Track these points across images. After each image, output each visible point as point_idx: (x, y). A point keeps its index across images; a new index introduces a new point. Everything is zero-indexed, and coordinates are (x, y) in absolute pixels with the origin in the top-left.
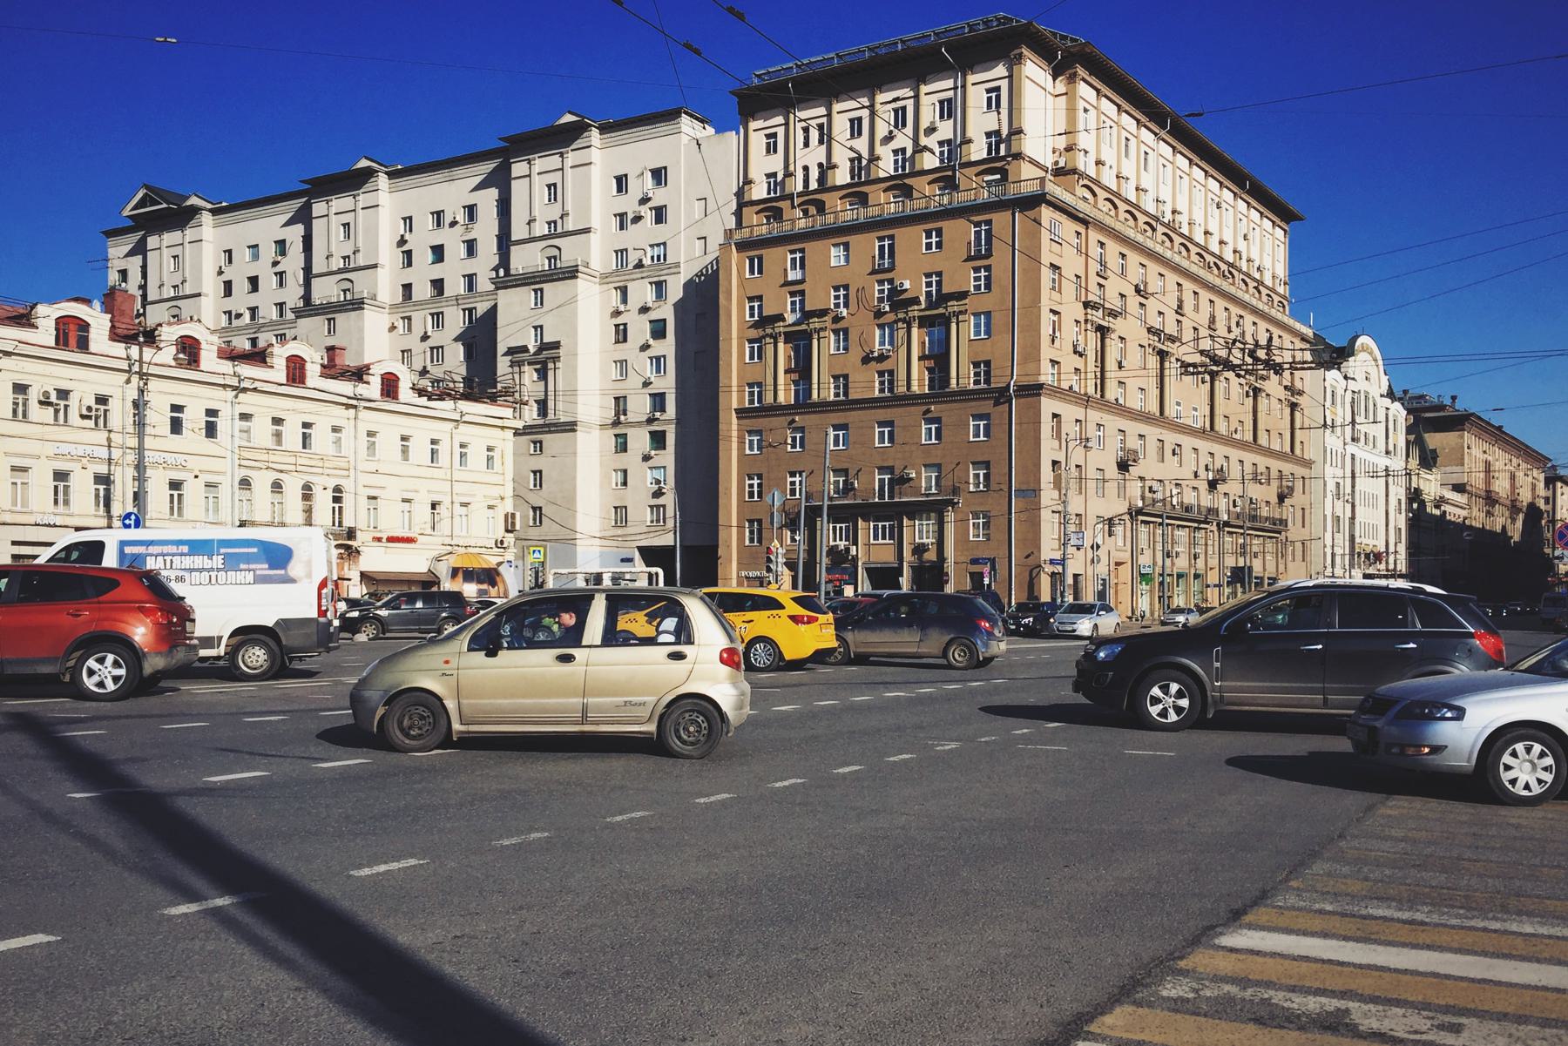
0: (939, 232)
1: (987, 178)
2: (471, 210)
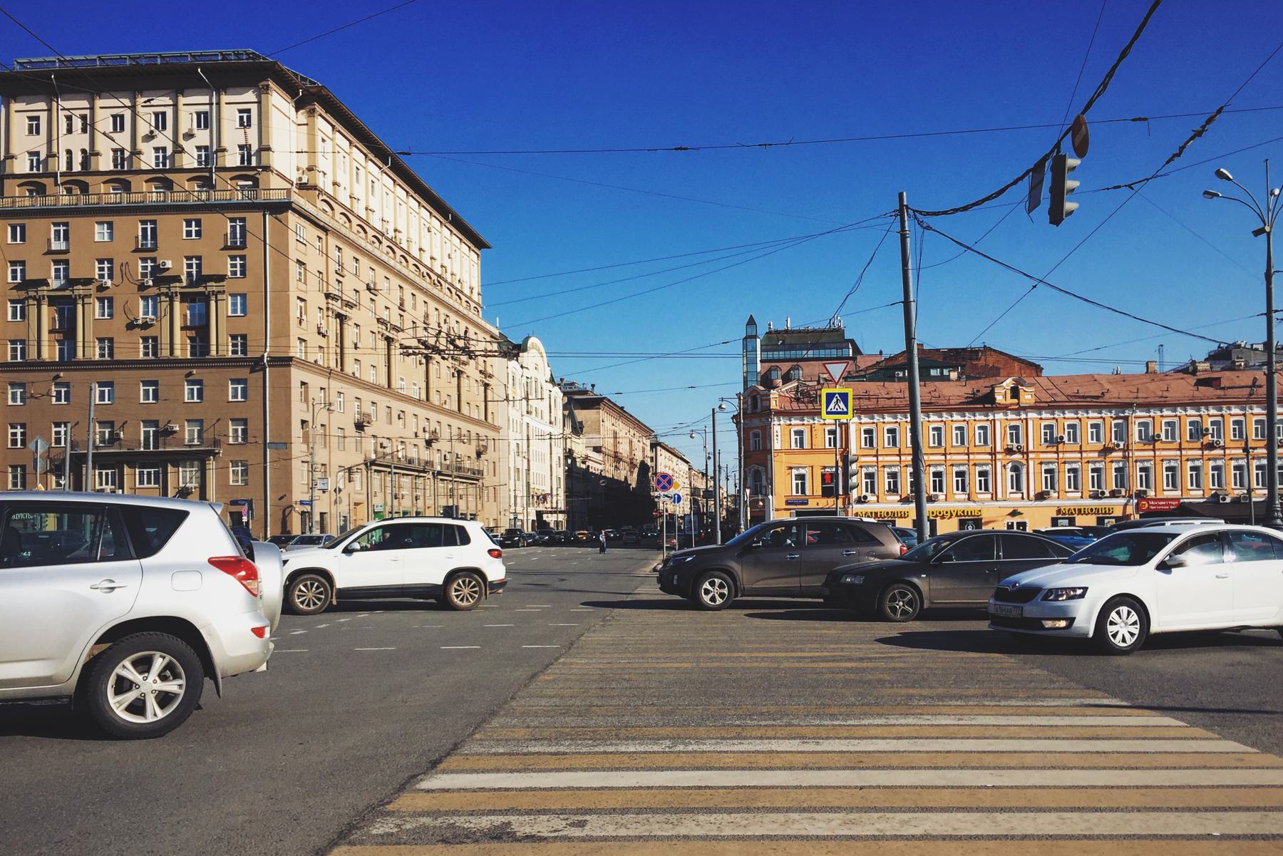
0: (198, 223)
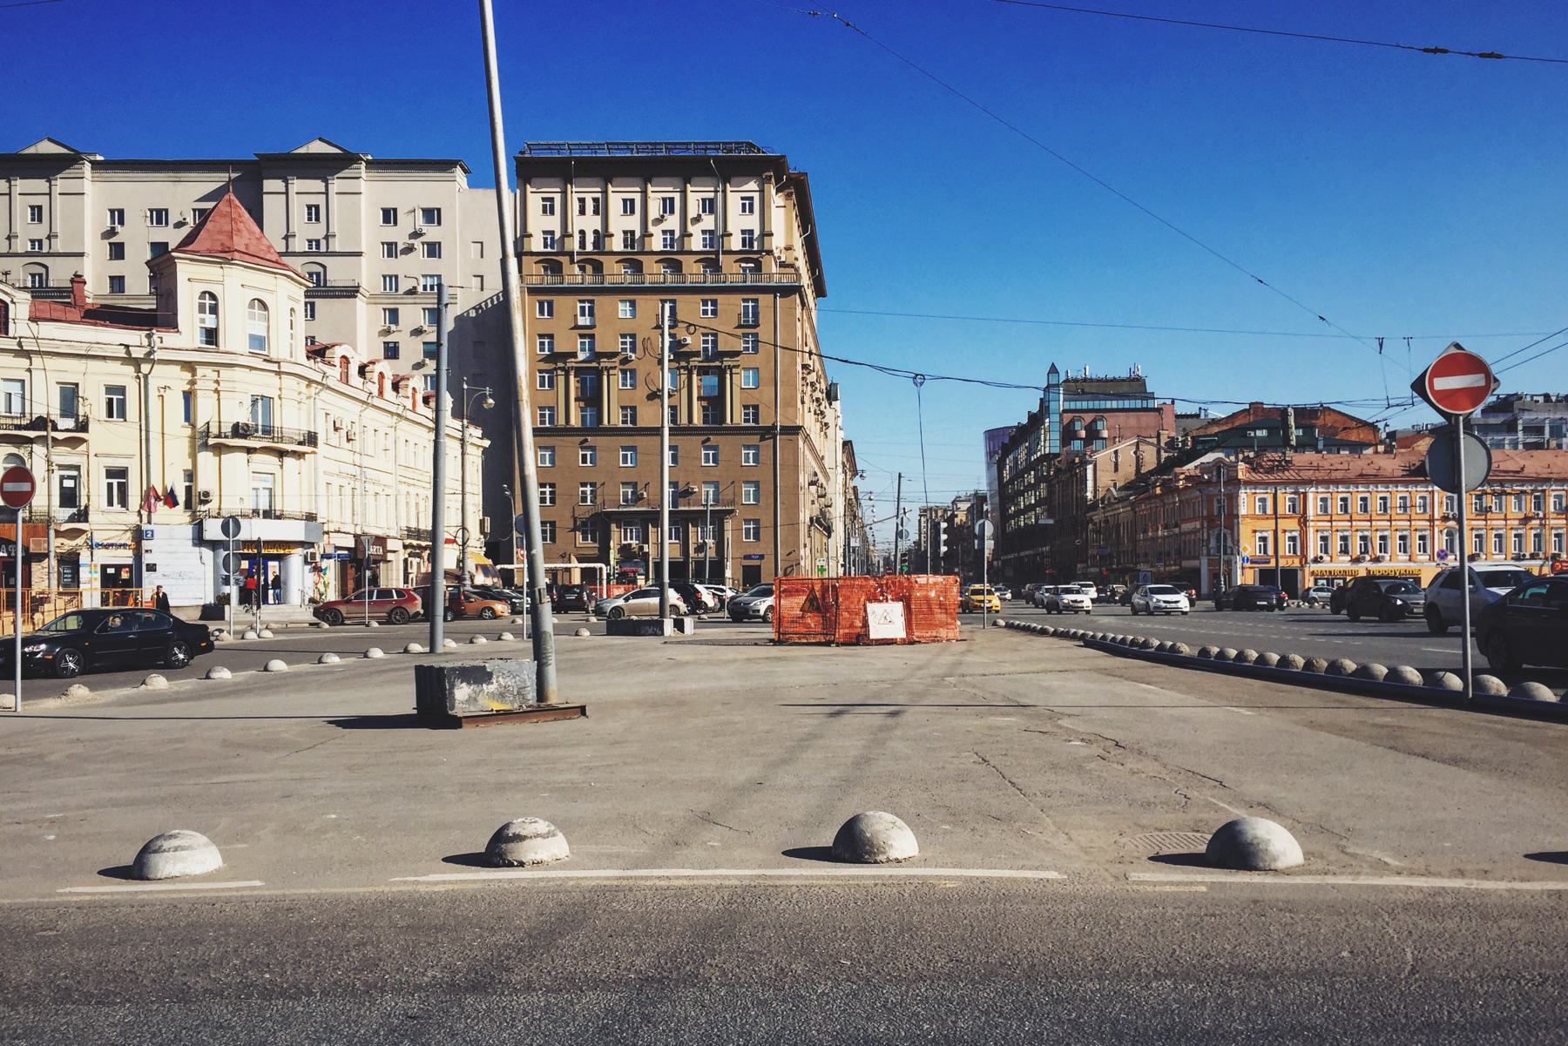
0: (714, 303)
1: (743, 265)
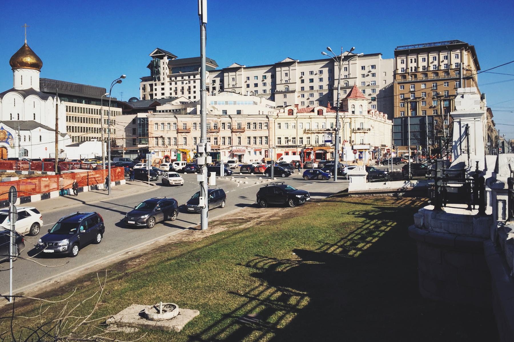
1: (456, 72)
2: (321, 72)
